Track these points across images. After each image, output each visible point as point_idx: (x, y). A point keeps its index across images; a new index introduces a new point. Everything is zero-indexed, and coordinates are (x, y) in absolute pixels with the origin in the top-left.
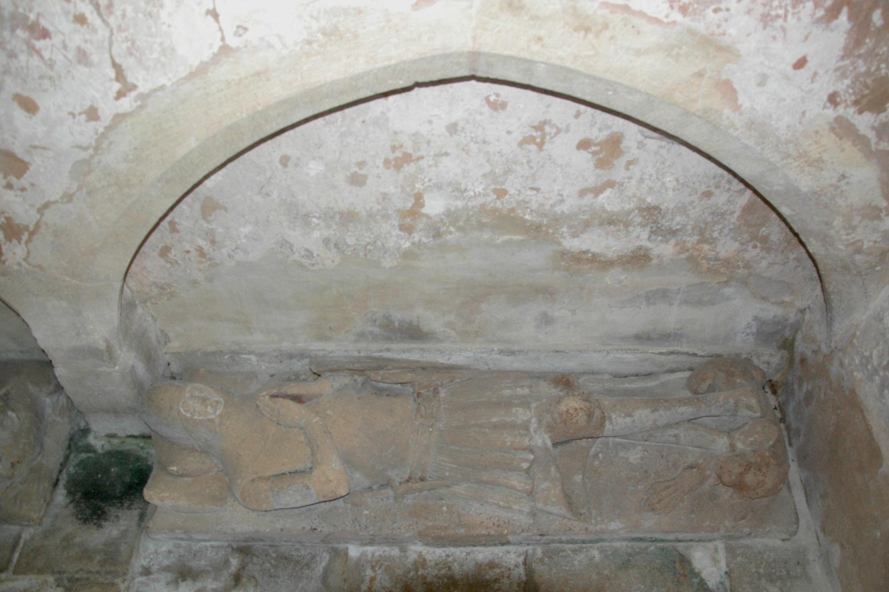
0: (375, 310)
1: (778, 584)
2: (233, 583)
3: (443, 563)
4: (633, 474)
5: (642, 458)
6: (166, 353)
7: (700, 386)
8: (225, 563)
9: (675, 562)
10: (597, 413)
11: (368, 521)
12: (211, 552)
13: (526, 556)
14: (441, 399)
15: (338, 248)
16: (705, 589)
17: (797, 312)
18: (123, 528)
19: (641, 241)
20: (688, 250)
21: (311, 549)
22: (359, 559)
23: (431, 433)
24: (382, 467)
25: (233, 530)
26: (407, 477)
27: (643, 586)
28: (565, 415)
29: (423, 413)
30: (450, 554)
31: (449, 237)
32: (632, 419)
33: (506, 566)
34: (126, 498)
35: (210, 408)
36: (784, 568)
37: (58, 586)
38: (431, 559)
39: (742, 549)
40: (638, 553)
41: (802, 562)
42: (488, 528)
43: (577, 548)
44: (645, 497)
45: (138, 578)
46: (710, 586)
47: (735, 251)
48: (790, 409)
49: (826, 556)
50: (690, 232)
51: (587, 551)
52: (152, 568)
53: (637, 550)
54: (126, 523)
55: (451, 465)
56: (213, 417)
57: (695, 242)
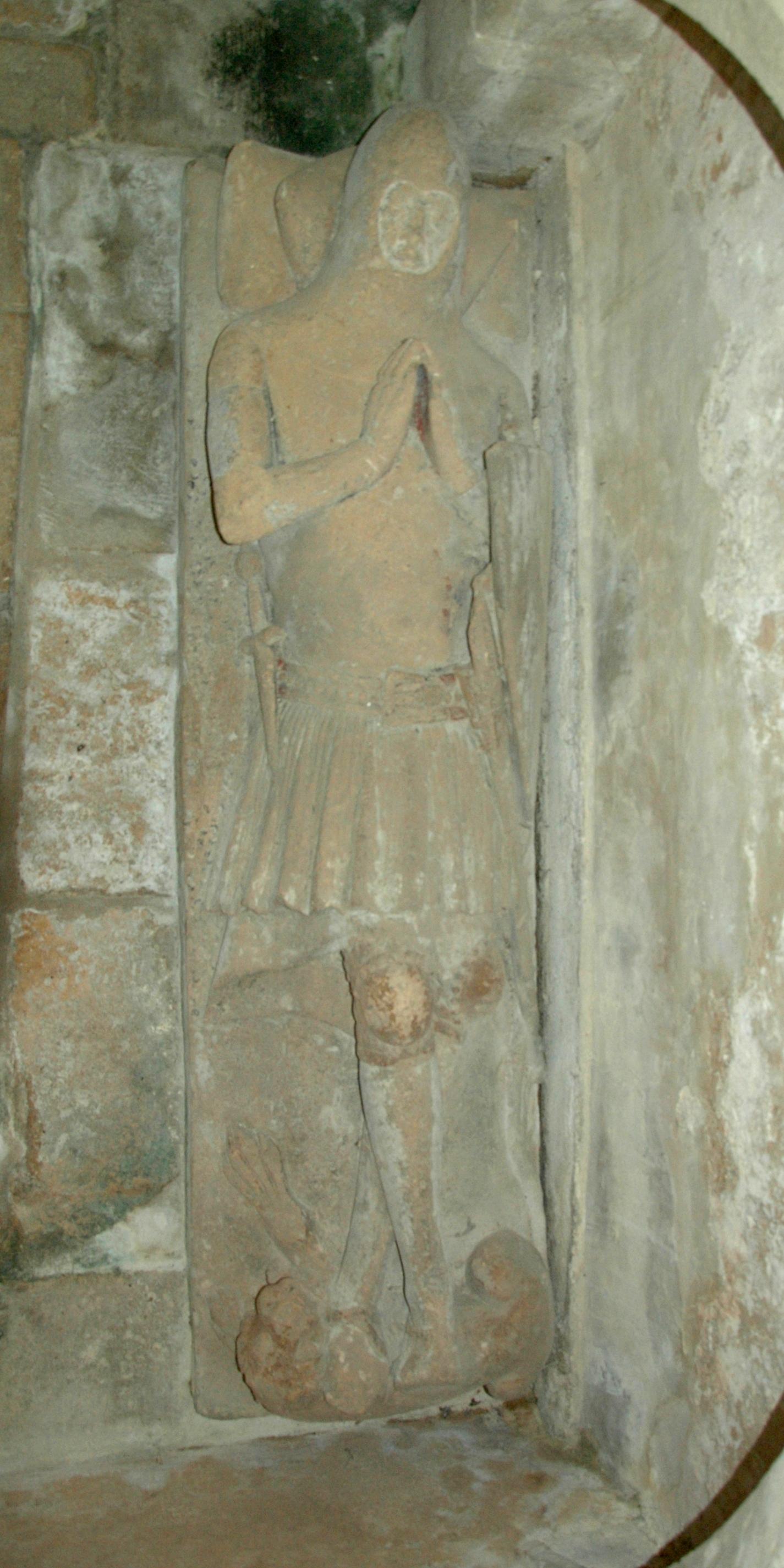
0: (641, 577)
1: (104, 1362)
2: (99, 341)
3: (144, 735)
4: (300, 1112)
5: (329, 1132)
6: (564, 147)
7: (484, 1264)
8: (139, 321)
9: (146, 1175)
10: (392, 1050)
11: (209, 588)
12: (159, 293)
13: (158, 895)
14: (438, 724)
15: (732, 478)
16: (93, 1226)
17: (634, 1489)
18: (206, 120)
19: (746, 1179)
20: (730, 1281)
21: (169, 483)
22: (151, 576)
23: (362, 704)
24: (296, 607)
25: (189, 329)
26: (288, 660)
27: (98, 1111)
28: (381, 984)
29: (405, 688)
30: (163, 749)
31: (753, 732)
32: (384, 1121)
33: (137, 856)
34: (268, 117)
35: (401, 245)
36: (135, 1377)
37: (90, 16)
38: (152, 713)
39: (171, 1304)
40: (164, 1107)
41: (145, 1414)
42: (197, 820)
43: (174, 991)
44: (254, 1131)
45: (108, 163)
46: (98, 1237)
47: (728, 1388)
48: (463, 1436)
49: (154, 1458)
50: (760, 1295)
51: (169, 1012)
52: (127, 186)
53: (171, 1106)
54: (218, 124)
55: (299, 747)
56: (386, 254)
57: (743, 1301)
